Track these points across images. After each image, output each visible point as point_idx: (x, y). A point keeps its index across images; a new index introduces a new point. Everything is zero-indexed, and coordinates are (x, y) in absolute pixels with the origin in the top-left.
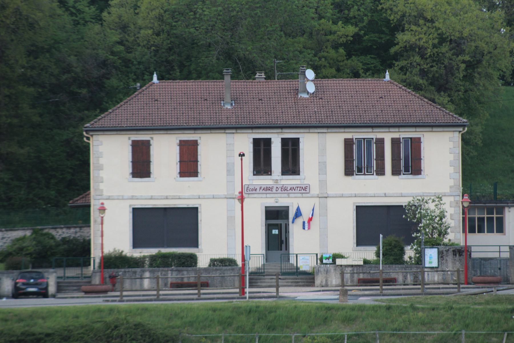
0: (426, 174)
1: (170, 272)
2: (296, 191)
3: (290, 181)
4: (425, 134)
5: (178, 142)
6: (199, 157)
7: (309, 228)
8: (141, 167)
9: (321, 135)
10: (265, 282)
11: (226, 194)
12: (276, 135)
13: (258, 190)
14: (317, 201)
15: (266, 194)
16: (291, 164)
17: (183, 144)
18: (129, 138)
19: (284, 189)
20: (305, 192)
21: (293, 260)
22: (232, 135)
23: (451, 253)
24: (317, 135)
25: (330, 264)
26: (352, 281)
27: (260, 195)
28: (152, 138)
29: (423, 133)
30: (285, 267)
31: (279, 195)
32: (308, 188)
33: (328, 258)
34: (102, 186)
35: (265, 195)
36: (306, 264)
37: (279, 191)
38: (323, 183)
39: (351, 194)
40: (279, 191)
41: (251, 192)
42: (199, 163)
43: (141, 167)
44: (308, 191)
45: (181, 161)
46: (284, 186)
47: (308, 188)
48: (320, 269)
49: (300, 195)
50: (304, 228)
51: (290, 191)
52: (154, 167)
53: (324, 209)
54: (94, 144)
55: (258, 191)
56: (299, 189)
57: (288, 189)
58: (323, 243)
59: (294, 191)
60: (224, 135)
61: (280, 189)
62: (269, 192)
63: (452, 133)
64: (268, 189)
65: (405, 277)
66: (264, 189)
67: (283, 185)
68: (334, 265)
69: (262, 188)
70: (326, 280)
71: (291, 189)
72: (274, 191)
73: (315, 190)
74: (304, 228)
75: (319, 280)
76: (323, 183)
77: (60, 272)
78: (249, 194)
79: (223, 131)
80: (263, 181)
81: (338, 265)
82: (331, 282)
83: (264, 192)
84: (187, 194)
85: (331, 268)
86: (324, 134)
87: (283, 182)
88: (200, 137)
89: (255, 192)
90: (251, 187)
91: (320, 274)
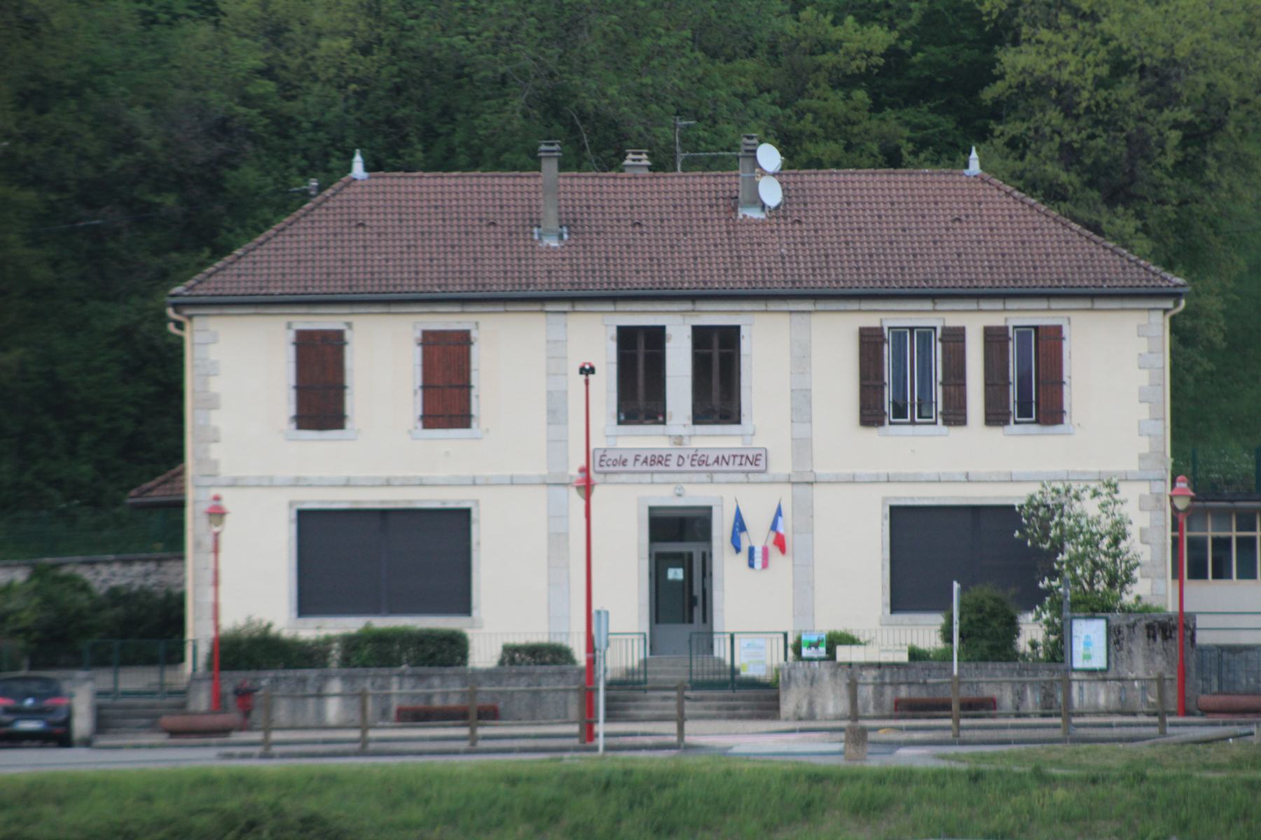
2: (731, 467)
3: (716, 439)
4: (1073, 315)
5: (418, 335)
8: (320, 399)
9: (797, 317)
10: (647, 708)
11: (545, 472)
12: (678, 319)
14: (784, 494)
15: (652, 473)
16: (719, 396)
18: (289, 326)
19: (700, 460)
20: (753, 468)
21: (721, 650)
23: (1141, 633)
25: (821, 660)
27: (636, 478)
28: (349, 325)
31: (685, 477)
32: (763, 458)
34: (215, 452)
35: (648, 478)
36: (756, 658)
37: (687, 466)
38: (802, 447)
39: (878, 475)
40: (687, 466)
41: (612, 468)
43: (320, 399)
44: (762, 467)
45: (427, 387)
46: (700, 453)
47: (763, 458)
48: (793, 673)
49: (741, 477)
50: (751, 565)
51: (716, 467)
52: (354, 403)
53: (806, 511)
54: (197, 340)
55: (630, 466)
56: (738, 460)
57: (711, 461)
58: (804, 587)
59: (724, 467)
60: (542, 317)
61: (688, 462)
63: (1146, 314)
64: (657, 460)
65: (1020, 696)
66: (645, 461)
67: (697, 450)
68: (830, 663)
69: (642, 459)
71: (717, 461)
72: (673, 465)
73: (781, 464)
74: (751, 565)
75: (790, 702)
76: (802, 447)
77: (104, 679)
78: (606, 473)
79: (537, 307)
80: (644, 438)
81: (841, 664)
82: (824, 709)
83: (645, 468)
84: (441, 473)
85: (824, 670)
86: (805, 316)
87: (697, 443)
88: (477, 323)
89: (620, 468)
91: (793, 686)
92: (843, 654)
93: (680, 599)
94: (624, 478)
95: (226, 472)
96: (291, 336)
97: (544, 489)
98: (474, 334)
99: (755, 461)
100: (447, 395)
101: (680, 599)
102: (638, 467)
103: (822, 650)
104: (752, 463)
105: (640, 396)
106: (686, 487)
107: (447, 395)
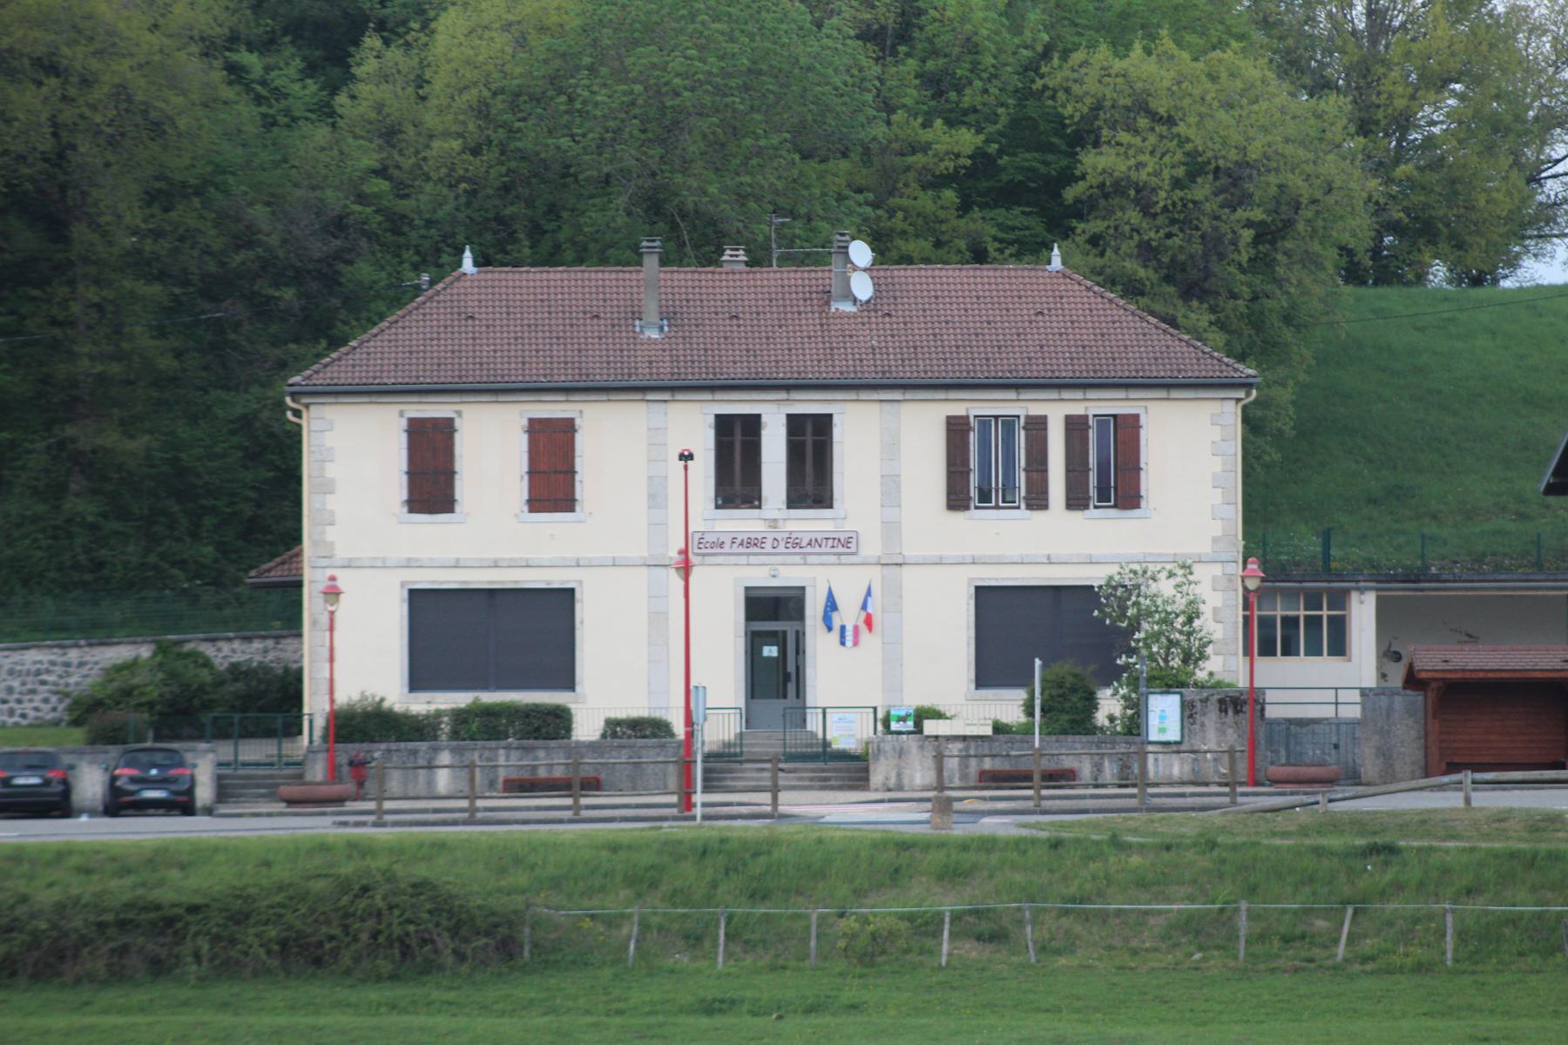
0: (1151, 506)
1: (502, 752)
2: (823, 550)
3: (809, 522)
4: (1150, 404)
5: (525, 422)
6: (577, 460)
7: (856, 643)
8: (431, 483)
9: (886, 406)
13: (727, 545)
15: (748, 554)
16: (812, 479)
17: (537, 429)
18: (401, 414)
19: (793, 543)
21: (814, 723)
22: (662, 406)
23: (1213, 708)
24: (876, 406)
26: (964, 776)
27: (733, 559)
28: (459, 413)
29: (457, 407)
30: (795, 741)
33: (903, 719)
34: (331, 534)
35: (743, 559)
36: (847, 733)
37: (781, 549)
38: (891, 529)
40: (781, 549)
42: (577, 478)
43: (431, 483)
44: (853, 550)
49: (833, 559)
50: (843, 643)
51: (809, 550)
52: (464, 488)
54: (313, 427)
55: (727, 549)
59: (817, 549)
60: (643, 406)
61: (782, 544)
62: (755, 550)
64: (753, 543)
65: (1098, 767)
70: (899, 775)
72: (768, 548)
73: (871, 546)
74: (843, 643)
75: (880, 773)
76: (891, 529)
78: (704, 555)
79: (639, 396)
80: (740, 521)
85: (911, 742)
86: (895, 405)
90: (709, 538)
92: (930, 727)
93: (775, 673)
94: (721, 559)
95: (341, 553)
96: (404, 423)
97: (645, 569)
98: (578, 422)
99: (846, 543)
100: (552, 481)
101: (775, 673)
102: (735, 549)
103: (910, 725)
104: (844, 544)
105: (736, 479)
106: (781, 568)
107: (552, 481)
